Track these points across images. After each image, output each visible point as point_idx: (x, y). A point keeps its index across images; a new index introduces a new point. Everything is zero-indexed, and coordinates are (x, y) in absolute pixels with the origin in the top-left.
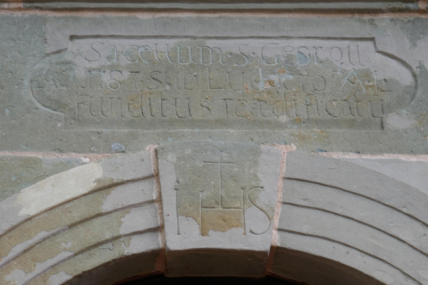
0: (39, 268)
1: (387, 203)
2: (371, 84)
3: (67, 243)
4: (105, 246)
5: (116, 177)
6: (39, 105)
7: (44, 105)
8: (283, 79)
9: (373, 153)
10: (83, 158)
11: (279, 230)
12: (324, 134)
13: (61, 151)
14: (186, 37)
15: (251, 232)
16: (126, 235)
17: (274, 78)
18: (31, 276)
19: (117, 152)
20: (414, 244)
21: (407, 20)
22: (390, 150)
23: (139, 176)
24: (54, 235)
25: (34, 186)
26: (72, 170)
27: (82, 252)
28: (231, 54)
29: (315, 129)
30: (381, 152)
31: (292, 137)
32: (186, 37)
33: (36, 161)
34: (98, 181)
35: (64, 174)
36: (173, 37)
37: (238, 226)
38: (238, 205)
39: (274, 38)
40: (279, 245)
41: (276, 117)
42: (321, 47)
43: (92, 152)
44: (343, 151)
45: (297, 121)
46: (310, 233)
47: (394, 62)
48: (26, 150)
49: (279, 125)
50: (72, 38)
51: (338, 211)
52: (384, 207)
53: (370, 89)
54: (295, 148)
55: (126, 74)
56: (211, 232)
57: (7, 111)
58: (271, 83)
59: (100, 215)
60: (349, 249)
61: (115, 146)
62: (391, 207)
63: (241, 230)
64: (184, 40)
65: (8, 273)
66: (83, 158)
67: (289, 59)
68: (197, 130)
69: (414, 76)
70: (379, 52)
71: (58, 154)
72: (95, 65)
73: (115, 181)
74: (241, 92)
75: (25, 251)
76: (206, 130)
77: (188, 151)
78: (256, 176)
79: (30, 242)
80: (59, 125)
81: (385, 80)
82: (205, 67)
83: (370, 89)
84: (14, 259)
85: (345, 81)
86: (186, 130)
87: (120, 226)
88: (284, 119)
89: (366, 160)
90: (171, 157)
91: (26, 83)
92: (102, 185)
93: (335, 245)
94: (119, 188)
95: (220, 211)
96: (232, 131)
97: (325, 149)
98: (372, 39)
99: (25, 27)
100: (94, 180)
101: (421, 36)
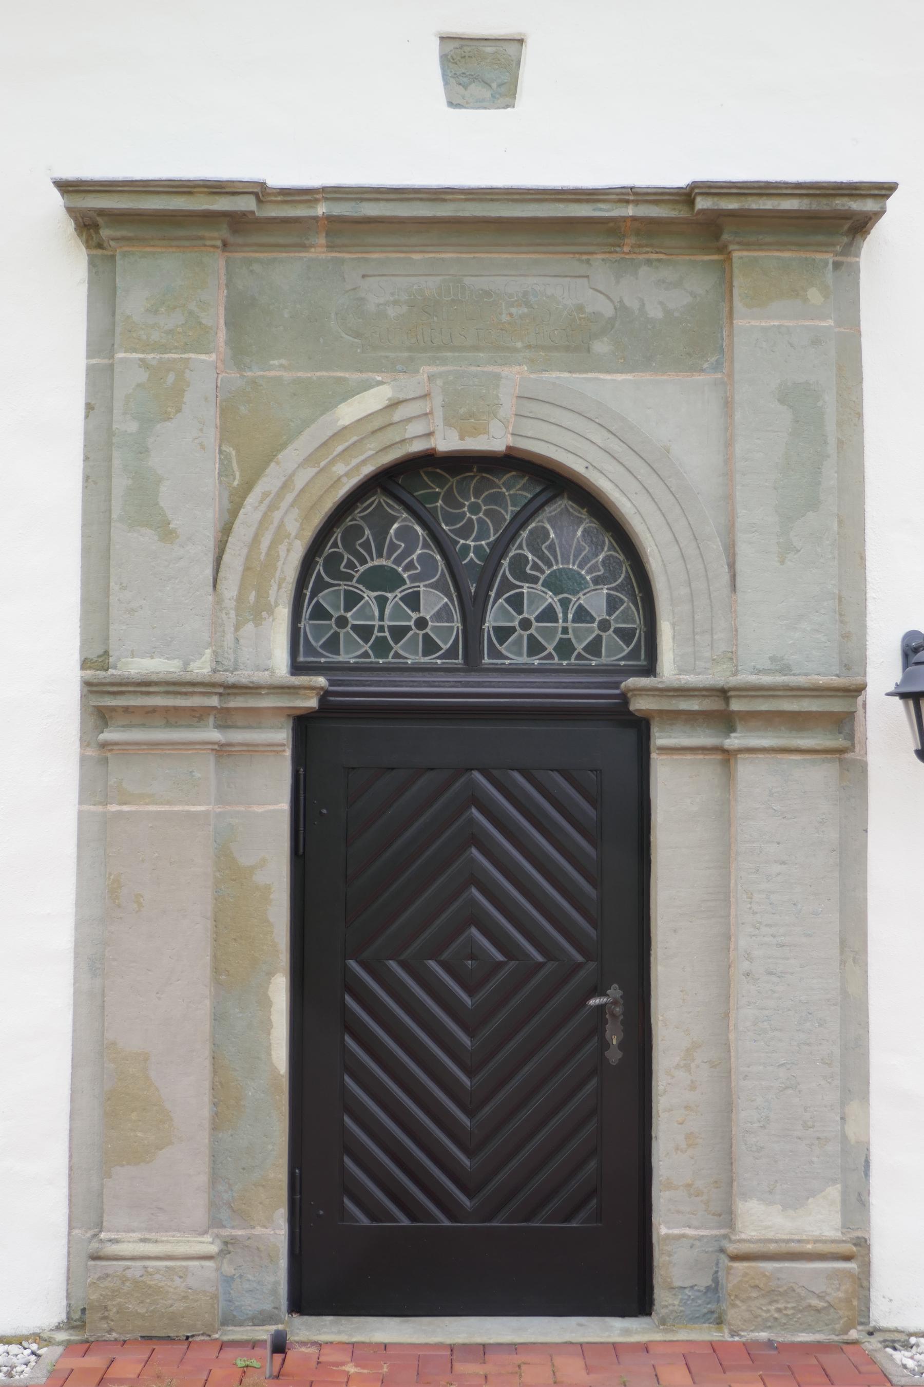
0: (355, 462)
1: (585, 415)
2: (583, 316)
3: (370, 444)
4: (396, 446)
5: (402, 396)
6: (343, 335)
7: (346, 334)
8: (520, 312)
9: (580, 372)
10: (376, 377)
11: (512, 434)
12: (547, 357)
13: (361, 372)
14: (449, 275)
15: (493, 437)
16: (409, 439)
17: (513, 310)
18: (349, 467)
19: (400, 372)
20: (601, 446)
21: (614, 260)
22: (591, 371)
23: (417, 395)
24: (362, 439)
25: (346, 403)
26: (372, 391)
27: (381, 450)
28: (482, 290)
29: (541, 353)
30: (586, 371)
31: (525, 360)
32: (449, 275)
33: (344, 379)
34: (389, 399)
35: (366, 394)
36: (439, 275)
37: (484, 433)
38: (485, 418)
39: (514, 276)
40: (511, 445)
41: (513, 344)
42: (549, 284)
43: (383, 372)
44: (560, 371)
45: (529, 347)
46: (532, 436)
47: (602, 296)
48: (337, 371)
49: (516, 350)
50: (364, 276)
51: (553, 421)
52: (584, 418)
53: (582, 320)
54: (526, 368)
55: (405, 308)
56: (467, 438)
57: (321, 340)
58: (511, 315)
59: (392, 424)
60: (557, 448)
61: (321, 190)
62: (588, 418)
63: (486, 436)
64: (447, 277)
65: (334, 466)
66: (376, 377)
67: (525, 294)
68: (457, 354)
69: (616, 309)
70: (591, 288)
71: (359, 374)
72: (382, 300)
73: (401, 399)
74: (488, 323)
75: (344, 451)
76: (464, 354)
77: (451, 378)
78: (498, 396)
79: (347, 444)
80: (359, 350)
81: (594, 313)
82: (462, 302)
83: (582, 320)
84: (337, 456)
85: (565, 313)
86: (449, 354)
87: (405, 432)
88: (519, 345)
89: (575, 378)
90: (439, 382)
91: (333, 316)
92: (392, 402)
93: (549, 445)
94: (404, 404)
95: (473, 422)
96: (481, 355)
97: (547, 369)
98: (587, 277)
99: (328, 267)
100: (386, 398)
101: (624, 275)
